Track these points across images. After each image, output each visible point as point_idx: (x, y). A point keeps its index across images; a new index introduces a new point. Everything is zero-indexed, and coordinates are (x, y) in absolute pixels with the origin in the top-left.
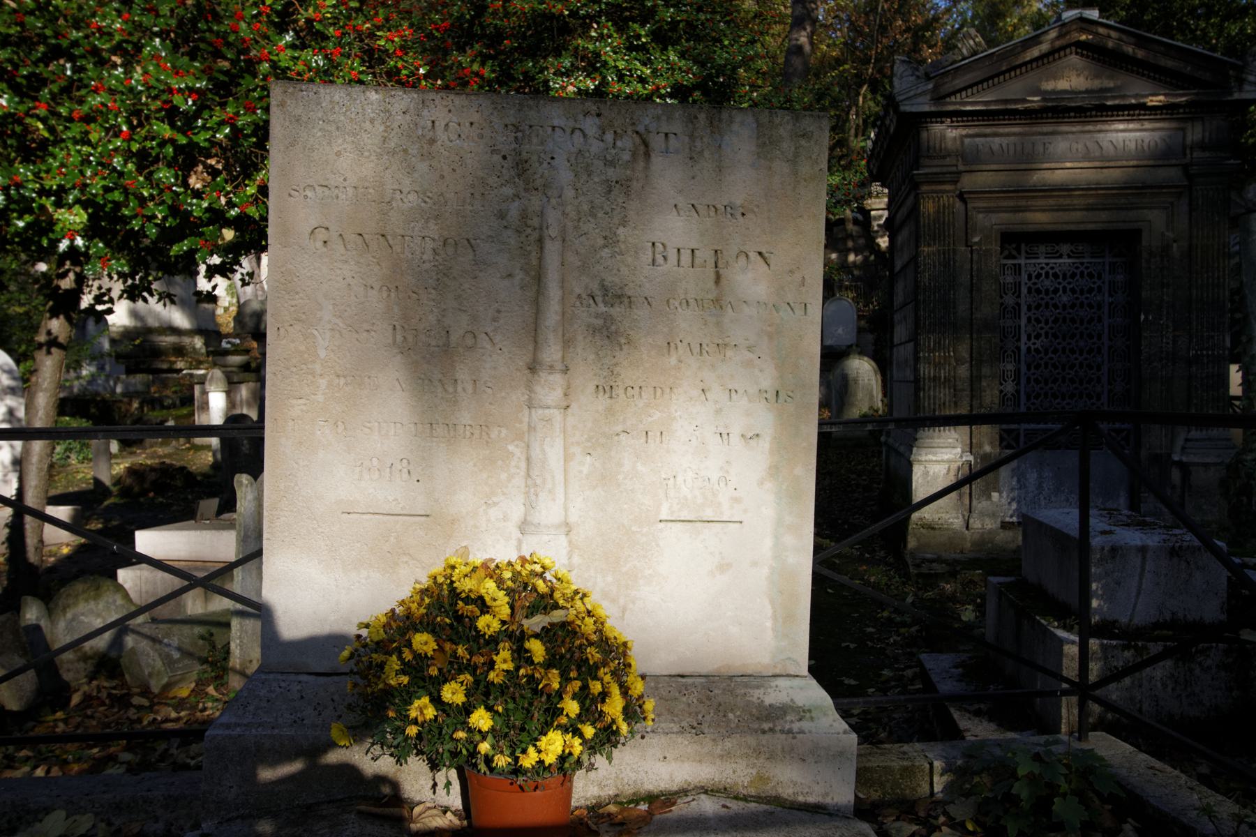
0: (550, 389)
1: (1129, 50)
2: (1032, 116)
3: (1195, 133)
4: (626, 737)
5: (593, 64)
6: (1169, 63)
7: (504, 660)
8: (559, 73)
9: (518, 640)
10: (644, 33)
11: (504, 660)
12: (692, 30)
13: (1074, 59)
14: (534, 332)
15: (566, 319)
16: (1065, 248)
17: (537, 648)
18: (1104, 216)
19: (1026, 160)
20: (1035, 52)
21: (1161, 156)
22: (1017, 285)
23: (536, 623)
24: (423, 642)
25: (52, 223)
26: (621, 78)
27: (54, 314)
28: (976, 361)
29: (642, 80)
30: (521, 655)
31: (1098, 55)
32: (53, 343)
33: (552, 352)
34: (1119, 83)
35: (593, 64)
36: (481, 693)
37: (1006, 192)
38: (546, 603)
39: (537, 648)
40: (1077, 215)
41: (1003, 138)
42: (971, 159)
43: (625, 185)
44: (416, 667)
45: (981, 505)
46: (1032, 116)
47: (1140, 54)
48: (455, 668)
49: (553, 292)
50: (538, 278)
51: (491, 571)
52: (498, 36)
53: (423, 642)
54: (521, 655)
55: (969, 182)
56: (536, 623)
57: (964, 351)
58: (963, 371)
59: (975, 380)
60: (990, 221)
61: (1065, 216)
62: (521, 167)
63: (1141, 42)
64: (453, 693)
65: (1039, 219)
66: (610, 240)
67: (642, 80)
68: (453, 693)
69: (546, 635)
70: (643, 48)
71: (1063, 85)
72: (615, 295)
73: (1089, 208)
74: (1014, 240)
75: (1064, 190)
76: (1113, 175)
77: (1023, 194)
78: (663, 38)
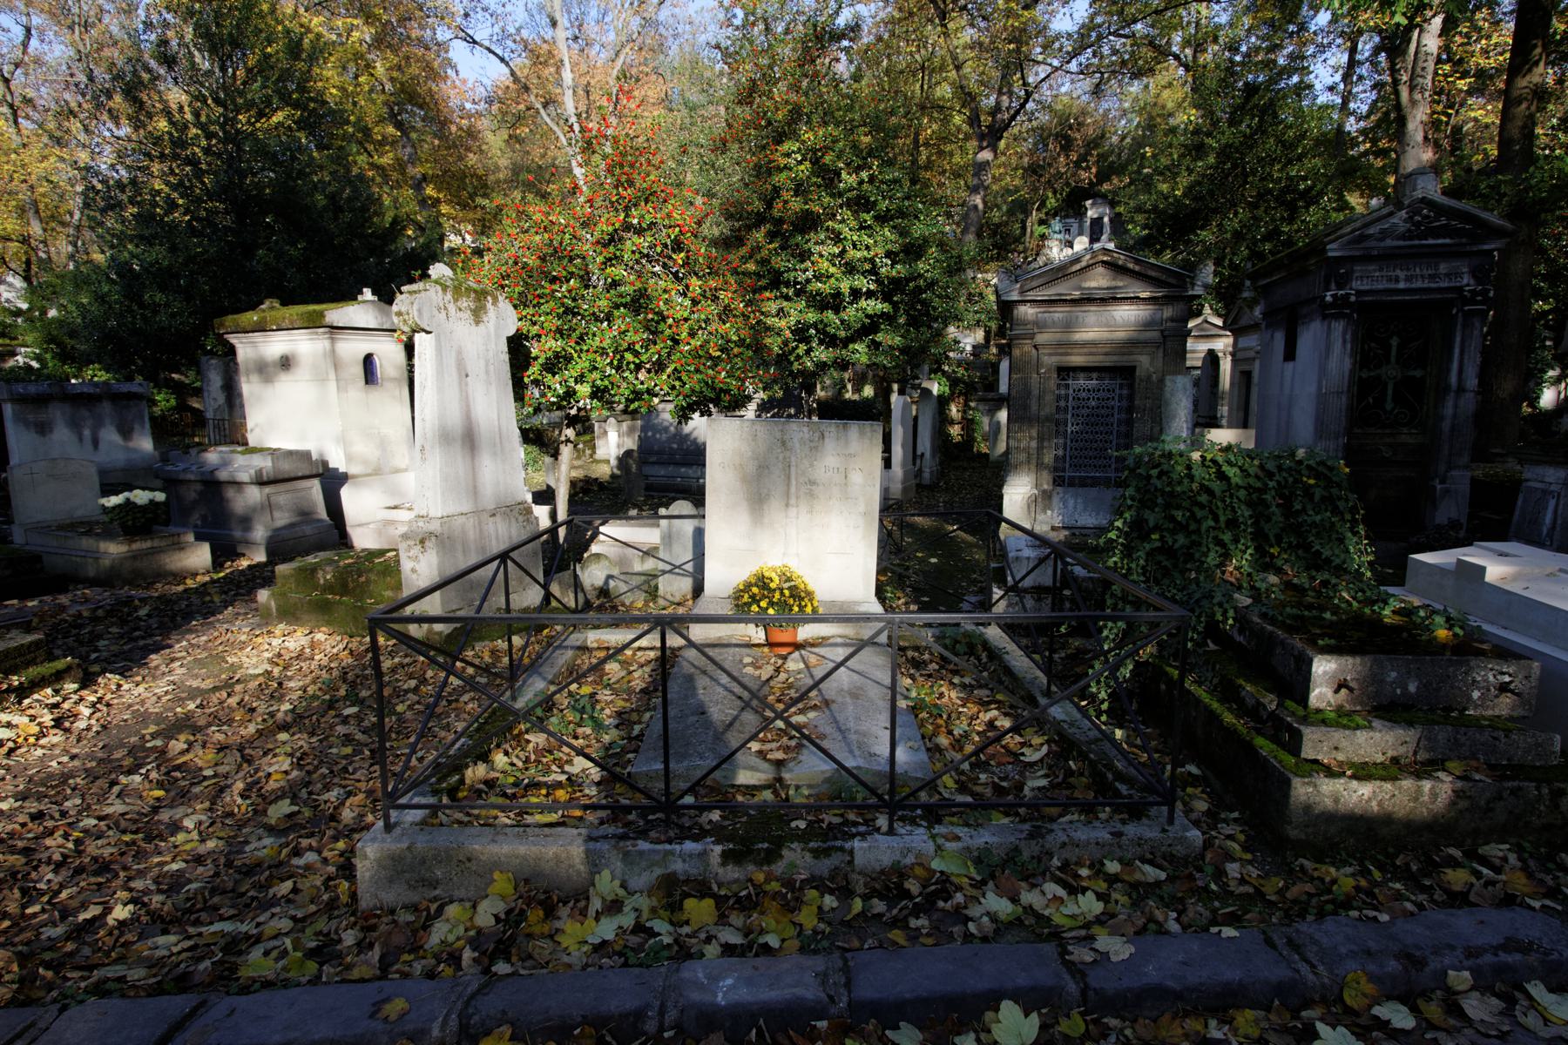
0: (793, 511)
1: (1131, 266)
2: (1074, 302)
3: (1168, 312)
4: (44, 242)
5: (837, 238)
6: (1153, 274)
7: (777, 595)
8: (816, 243)
9: (781, 590)
10: (868, 218)
11: (777, 595)
12: (902, 214)
13: (1100, 269)
14: (787, 495)
15: (798, 489)
16: (1095, 375)
17: (787, 593)
18: (1115, 358)
19: (1068, 326)
20: (1078, 267)
21: (1148, 325)
22: (1067, 396)
23: (787, 585)
24: (755, 590)
25: (575, 392)
26: (855, 246)
27: (568, 426)
28: (1041, 439)
29: (868, 248)
30: (782, 594)
31: (1114, 267)
32: (568, 441)
33: (793, 501)
34: (1120, 284)
35: (837, 238)
36: (771, 604)
37: (1060, 345)
38: (789, 580)
39: (787, 593)
40: (1101, 358)
41: (1059, 314)
42: (1040, 325)
43: (816, 448)
44: (753, 597)
45: (1041, 517)
46: (1074, 302)
47: (1137, 268)
48: (764, 596)
49: (793, 482)
50: (789, 478)
51: (774, 570)
52: (781, 221)
53: (755, 590)
54: (782, 594)
55: (1041, 338)
56: (787, 585)
57: (1034, 434)
58: (1034, 444)
59: (1040, 448)
60: (1050, 361)
61: (1091, 358)
62: (784, 443)
63: (1137, 261)
64: (763, 604)
65: (1077, 360)
66: (812, 465)
67: (868, 248)
68: (763, 604)
69: (790, 588)
70: (869, 227)
71: (1093, 284)
72: (813, 483)
73: (1106, 354)
74: (1065, 372)
75: (1093, 344)
76: (1121, 335)
77: (1065, 346)
78: (882, 219)
